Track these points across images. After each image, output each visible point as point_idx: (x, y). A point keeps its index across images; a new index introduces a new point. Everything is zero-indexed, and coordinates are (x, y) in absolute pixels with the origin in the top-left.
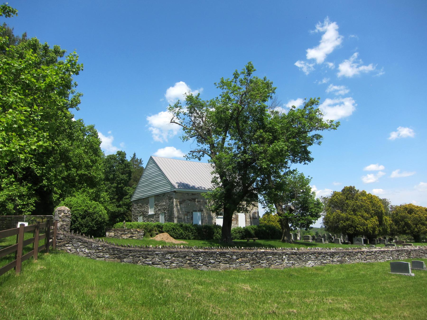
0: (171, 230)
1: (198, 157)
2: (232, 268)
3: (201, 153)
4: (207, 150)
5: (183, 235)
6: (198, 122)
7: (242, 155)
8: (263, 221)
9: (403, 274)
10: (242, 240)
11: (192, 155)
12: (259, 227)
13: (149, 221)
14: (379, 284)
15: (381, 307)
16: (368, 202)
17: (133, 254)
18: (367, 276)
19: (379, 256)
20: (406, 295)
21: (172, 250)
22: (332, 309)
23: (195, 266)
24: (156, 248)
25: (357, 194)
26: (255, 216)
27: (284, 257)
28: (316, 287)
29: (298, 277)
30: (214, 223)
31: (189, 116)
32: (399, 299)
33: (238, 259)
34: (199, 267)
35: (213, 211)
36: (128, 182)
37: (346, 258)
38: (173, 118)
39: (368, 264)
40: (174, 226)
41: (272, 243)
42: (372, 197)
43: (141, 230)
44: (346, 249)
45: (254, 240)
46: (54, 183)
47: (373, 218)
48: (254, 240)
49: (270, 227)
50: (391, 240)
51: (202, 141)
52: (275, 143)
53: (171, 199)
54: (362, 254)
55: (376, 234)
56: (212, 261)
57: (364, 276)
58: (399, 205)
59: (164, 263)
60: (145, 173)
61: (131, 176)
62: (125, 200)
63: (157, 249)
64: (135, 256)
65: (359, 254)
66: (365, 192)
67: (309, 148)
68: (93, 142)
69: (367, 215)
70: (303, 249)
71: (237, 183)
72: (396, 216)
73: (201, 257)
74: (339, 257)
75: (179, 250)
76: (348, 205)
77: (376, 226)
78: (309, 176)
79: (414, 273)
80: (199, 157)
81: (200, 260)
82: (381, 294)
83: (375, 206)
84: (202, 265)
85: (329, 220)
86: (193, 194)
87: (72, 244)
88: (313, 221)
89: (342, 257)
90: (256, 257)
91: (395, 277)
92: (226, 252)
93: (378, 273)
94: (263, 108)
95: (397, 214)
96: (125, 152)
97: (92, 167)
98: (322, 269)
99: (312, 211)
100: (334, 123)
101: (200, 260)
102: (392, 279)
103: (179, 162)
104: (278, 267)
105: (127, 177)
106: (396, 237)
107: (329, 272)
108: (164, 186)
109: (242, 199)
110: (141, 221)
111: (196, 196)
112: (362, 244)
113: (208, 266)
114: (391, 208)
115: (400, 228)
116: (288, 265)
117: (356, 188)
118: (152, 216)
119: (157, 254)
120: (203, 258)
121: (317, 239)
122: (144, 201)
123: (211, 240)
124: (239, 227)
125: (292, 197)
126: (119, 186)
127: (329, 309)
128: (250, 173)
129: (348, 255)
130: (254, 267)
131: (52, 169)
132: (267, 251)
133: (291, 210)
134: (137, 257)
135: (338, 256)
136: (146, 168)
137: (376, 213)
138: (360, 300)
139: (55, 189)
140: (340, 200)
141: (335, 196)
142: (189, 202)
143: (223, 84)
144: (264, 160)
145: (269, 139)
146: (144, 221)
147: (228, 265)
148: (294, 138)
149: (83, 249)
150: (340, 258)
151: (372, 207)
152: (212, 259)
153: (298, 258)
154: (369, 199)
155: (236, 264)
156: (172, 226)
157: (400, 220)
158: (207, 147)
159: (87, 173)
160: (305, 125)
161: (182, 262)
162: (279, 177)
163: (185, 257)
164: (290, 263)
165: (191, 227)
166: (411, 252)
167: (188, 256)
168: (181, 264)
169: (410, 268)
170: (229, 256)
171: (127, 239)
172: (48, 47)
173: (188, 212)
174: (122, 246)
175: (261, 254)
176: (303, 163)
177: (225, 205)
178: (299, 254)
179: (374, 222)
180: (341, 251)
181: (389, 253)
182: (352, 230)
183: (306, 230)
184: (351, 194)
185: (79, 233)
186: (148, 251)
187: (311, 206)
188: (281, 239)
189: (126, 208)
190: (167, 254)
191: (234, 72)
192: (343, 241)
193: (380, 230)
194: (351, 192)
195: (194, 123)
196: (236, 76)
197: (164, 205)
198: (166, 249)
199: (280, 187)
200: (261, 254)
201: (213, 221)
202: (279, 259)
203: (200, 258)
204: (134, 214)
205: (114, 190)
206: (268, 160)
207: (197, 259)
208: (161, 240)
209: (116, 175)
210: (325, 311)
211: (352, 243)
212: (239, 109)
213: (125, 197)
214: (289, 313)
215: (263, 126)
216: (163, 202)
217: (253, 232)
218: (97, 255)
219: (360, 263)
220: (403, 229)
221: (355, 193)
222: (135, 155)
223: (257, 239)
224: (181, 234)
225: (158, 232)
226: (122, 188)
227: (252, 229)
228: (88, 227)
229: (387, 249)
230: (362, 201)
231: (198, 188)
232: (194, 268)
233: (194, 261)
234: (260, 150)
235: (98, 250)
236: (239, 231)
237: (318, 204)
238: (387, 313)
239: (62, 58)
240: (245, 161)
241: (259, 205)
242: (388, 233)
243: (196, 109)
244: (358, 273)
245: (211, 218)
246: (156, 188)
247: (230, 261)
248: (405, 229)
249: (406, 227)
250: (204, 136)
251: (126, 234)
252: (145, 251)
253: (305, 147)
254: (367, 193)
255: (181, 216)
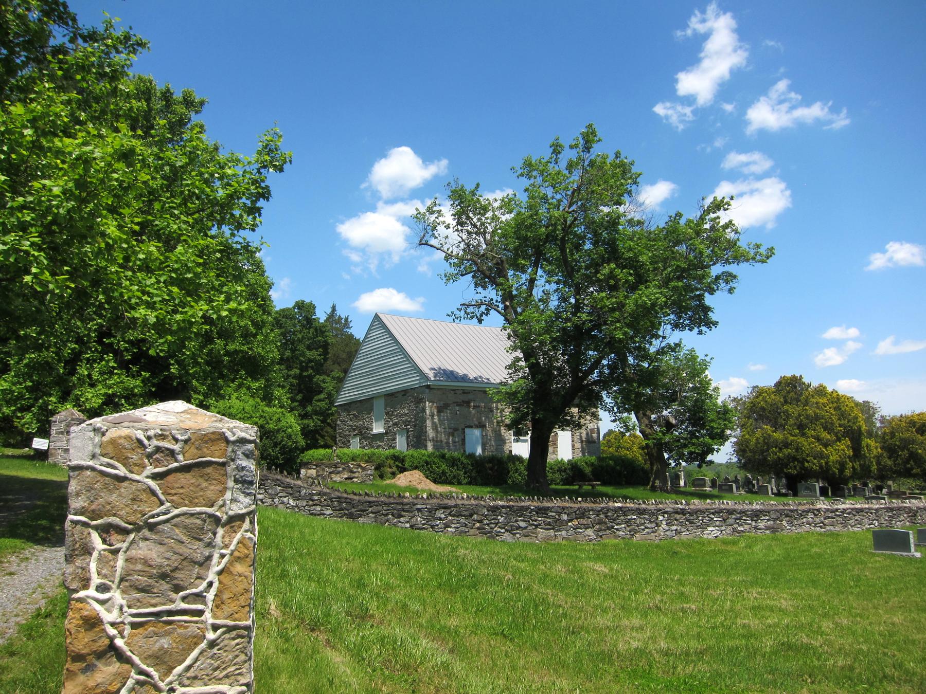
0: (423, 466)
1: (477, 317)
2: (559, 540)
3: (483, 308)
4: (494, 301)
5: (448, 475)
6: (475, 243)
7: (574, 314)
8: (605, 448)
9: (899, 553)
10: (567, 487)
11: (465, 312)
12: (600, 459)
13: (373, 447)
14: (849, 570)
15: (851, 608)
16: (830, 408)
17: (375, 509)
18: (826, 556)
19: (850, 519)
20: (901, 589)
21: (446, 501)
22: (759, 607)
23: (489, 532)
24: (417, 497)
25: (807, 393)
26: (592, 436)
27: (661, 518)
28: (726, 572)
29: (689, 556)
30: (508, 452)
31: (457, 230)
32: (886, 596)
33: (570, 521)
34: (497, 535)
35: (509, 427)
36: (322, 365)
37: (784, 523)
38: (424, 236)
39: (828, 535)
40: (429, 456)
41: (630, 491)
42: (838, 399)
43: (368, 465)
44: (784, 505)
45: (593, 486)
46: (191, 371)
47: (840, 442)
48: (593, 486)
49: (623, 461)
50: (880, 488)
51: (486, 283)
52: (641, 290)
53: (419, 401)
54: (815, 515)
55: (845, 475)
56: (522, 524)
57: (820, 555)
58: (898, 415)
59: (432, 527)
60: (364, 350)
61: (328, 353)
62: (319, 403)
63: (419, 501)
64: (379, 512)
65: (810, 515)
66: (825, 388)
67: (708, 300)
68: (257, 284)
69: (829, 437)
70: (697, 503)
71: (560, 369)
72: (891, 439)
73: (502, 516)
74: (768, 520)
75: (459, 502)
76: (788, 416)
77: (848, 460)
78: (706, 355)
79: (921, 552)
80: (478, 315)
81: (498, 523)
82: (851, 587)
83: (845, 418)
84: (503, 531)
85: (747, 447)
86: (465, 392)
87: (265, 490)
88: (716, 447)
89: (776, 519)
90: (606, 517)
91: (881, 558)
92: (548, 507)
93: (848, 550)
94: (615, 219)
95: (892, 434)
96: (313, 303)
97: (255, 336)
98: (734, 543)
99: (712, 428)
100: (762, 250)
101: (498, 523)
102: (876, 562)
103: (433, 324)
104: (648, 537)
105: (320, 355)
106: (890, 483)
107: (750, 548)
108: (405, 374)
109: (570, 404)
110: (355, 446)
111: (470, 396)
112: (816, 496)
113: (514, 534)
114: (882, 422)
115: (899, 464)
116: (669, 533)
117: (806, 380)
118: (379, 436)
119: (419, 510)
120: (505, 518)
121: (723, 487)
122: (363, 406)
123: (504, 486)
124: (560, 459)
125: (673, 398)
126: (305, 374)
127: (754, 608)
128: (588, 349)
129: (787, 516)
130: (601, 537)
131: (186, 343)
132: (628, 505)
133: (669, 426)
134: (383, 515)
135: (767, 518)
136: (366, 338)
137: (848, 432)
138: (810, 595)
139: (194, 382)
140: (771, 405)
141: (760, 395)
142: (457, 408)
143: (529, 167)
144: (618, 325)
145: (627, 281)
146: (363, 447)
147: (552, 533)
148: (679, 278)
149: (285, 500)
150: (772, 522)
151: (839, 419)
152: (521, 520)
153: (687, 521)
154: (832, 403)
155: (567, 531)
156: (424, 458)
157: (899, 447)
158: (491, 293)
159: (245, 348)
160: (701, 253)
161: (466, 524)
162: (645, 356)
163: (471, 515)
164: (672, 531)
165: (463, 458)
166: (917, 512)
167: (477, 514)
168: (463, 529)
169: (912, 541)
170: (554, 514)
171: (340, 482)
172: (172, 94)
173: (456, 430)
174: (355, 494)
175: (616, 512)
176: (696, 330)
177: (534, 413)
178: (689, 513)
179: (843, 450)
180: (774, 508)
181: (871, 513)
182: (795, 467)
183: (700, 466)
184: (795, 393)
185: (276, 469)
186: (402, 504)
187: (711, 416)
188: (648, 484)
189: (318, 419)
190: (437, 509)
191: (551, 141)
192: (775, 491)
193: (856, 467)
194: (795, 387)
195: (468, 245)
196: (557, 149)
197: (406, 414)
198: (435, 501)
199: (649, 378)
200: (616, 512)
201: (506, 448)
202: (651, 522)
203: (499, 517)
204: (340, 433)
205: (295, 381)
206: (627, 325)
207: (494, 519)
208: (408, 484)
209: (299, 350)
210: (747, 609)
211: (795, 494)
212: (566, 221)
213: (316, 398)
214: (683, 610)
215: (613, 254)
216: (403, 408)
217: (588, 470)
218: (309, 510)
219: (813, 533)
220: (905, 466)
221: (802, 389)
222: (334, 308)
223: (598, 485)
224: (444, 473)
225: (394, 469)
226: (310, 377)
227: (586, 463)
228: (267, 459)
229: (867, 506)
230: (818, 408)
231: (476, 378)
232: (489, 537)
233: (488, 525)
234: (612, 304)
235: (313, 500)
236: (561, 467)
237: (724, 413)
238: (861, 617)
239: (199, 115)
240: (577, 328)
241: (602, 414)
242: (872, 474)
243: (471, 215)
244: (808, 551)
245: (501, 441)
246: (387, 379)
247: (557, 525)
248: (909, 466)
249: (912, 462)
250: (488, 273)
251: (339, 473)
252: (397, 504)
253: (700, 298)
254: (829, 389)
255: (441, 438)
